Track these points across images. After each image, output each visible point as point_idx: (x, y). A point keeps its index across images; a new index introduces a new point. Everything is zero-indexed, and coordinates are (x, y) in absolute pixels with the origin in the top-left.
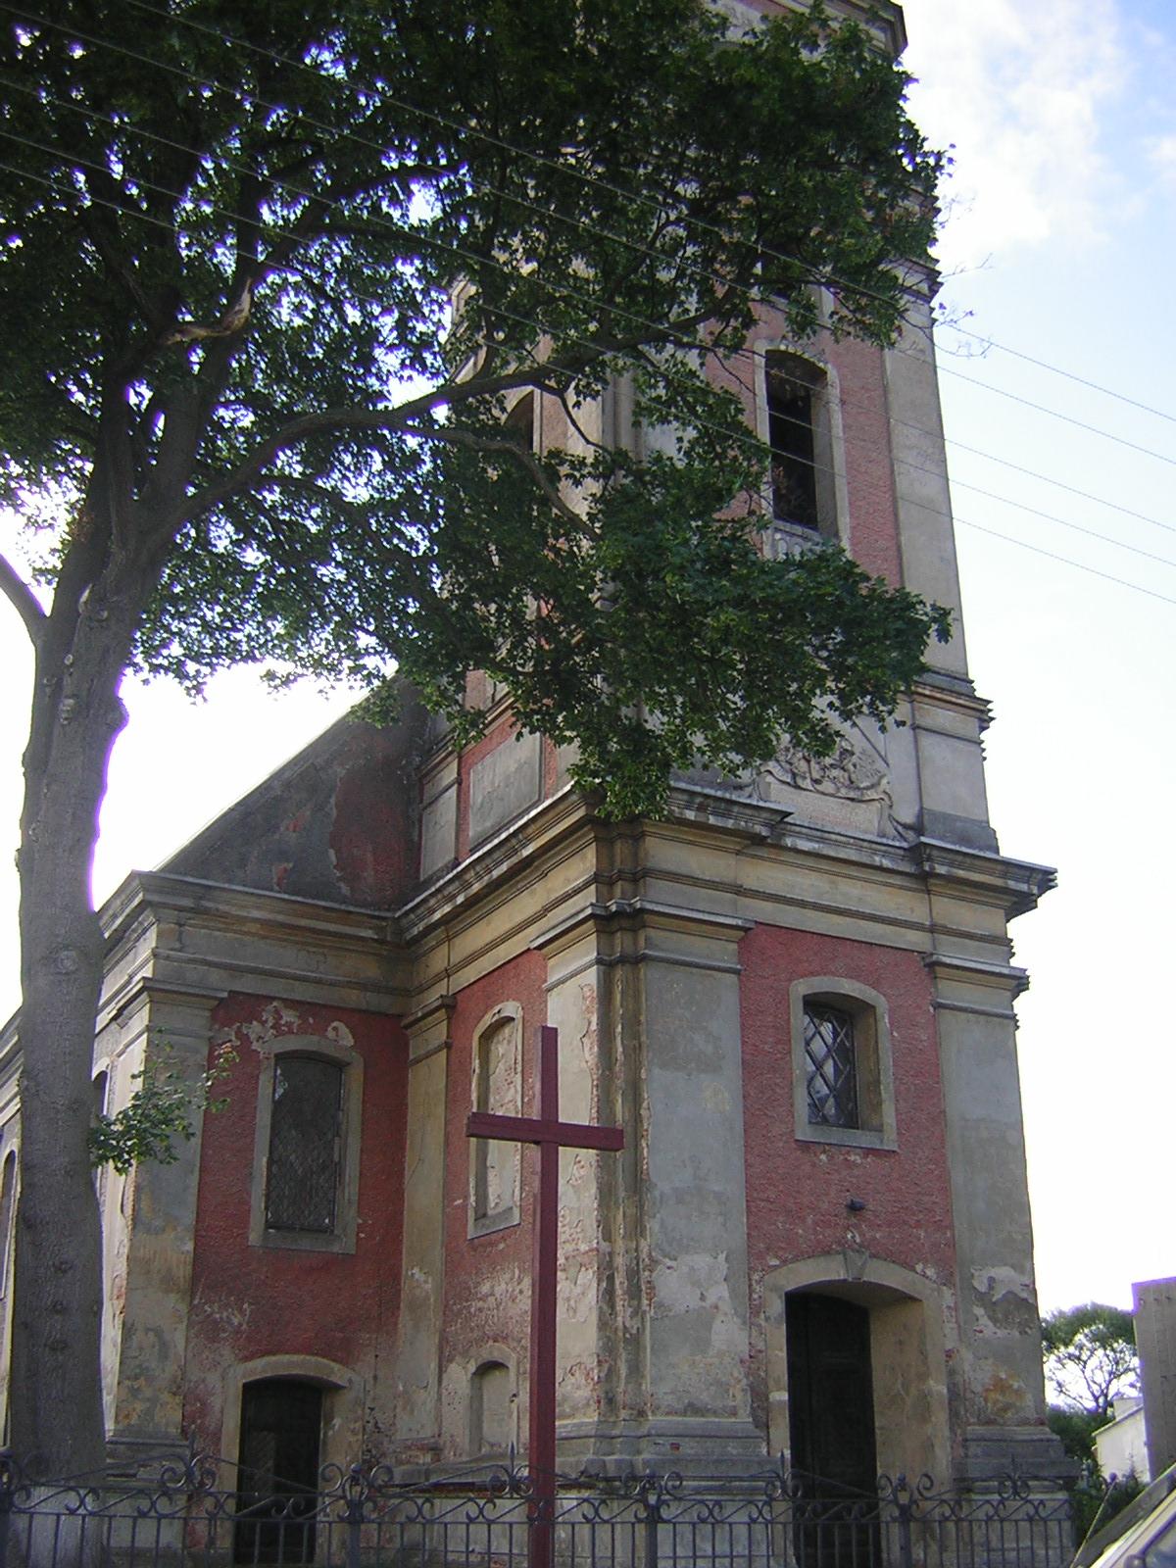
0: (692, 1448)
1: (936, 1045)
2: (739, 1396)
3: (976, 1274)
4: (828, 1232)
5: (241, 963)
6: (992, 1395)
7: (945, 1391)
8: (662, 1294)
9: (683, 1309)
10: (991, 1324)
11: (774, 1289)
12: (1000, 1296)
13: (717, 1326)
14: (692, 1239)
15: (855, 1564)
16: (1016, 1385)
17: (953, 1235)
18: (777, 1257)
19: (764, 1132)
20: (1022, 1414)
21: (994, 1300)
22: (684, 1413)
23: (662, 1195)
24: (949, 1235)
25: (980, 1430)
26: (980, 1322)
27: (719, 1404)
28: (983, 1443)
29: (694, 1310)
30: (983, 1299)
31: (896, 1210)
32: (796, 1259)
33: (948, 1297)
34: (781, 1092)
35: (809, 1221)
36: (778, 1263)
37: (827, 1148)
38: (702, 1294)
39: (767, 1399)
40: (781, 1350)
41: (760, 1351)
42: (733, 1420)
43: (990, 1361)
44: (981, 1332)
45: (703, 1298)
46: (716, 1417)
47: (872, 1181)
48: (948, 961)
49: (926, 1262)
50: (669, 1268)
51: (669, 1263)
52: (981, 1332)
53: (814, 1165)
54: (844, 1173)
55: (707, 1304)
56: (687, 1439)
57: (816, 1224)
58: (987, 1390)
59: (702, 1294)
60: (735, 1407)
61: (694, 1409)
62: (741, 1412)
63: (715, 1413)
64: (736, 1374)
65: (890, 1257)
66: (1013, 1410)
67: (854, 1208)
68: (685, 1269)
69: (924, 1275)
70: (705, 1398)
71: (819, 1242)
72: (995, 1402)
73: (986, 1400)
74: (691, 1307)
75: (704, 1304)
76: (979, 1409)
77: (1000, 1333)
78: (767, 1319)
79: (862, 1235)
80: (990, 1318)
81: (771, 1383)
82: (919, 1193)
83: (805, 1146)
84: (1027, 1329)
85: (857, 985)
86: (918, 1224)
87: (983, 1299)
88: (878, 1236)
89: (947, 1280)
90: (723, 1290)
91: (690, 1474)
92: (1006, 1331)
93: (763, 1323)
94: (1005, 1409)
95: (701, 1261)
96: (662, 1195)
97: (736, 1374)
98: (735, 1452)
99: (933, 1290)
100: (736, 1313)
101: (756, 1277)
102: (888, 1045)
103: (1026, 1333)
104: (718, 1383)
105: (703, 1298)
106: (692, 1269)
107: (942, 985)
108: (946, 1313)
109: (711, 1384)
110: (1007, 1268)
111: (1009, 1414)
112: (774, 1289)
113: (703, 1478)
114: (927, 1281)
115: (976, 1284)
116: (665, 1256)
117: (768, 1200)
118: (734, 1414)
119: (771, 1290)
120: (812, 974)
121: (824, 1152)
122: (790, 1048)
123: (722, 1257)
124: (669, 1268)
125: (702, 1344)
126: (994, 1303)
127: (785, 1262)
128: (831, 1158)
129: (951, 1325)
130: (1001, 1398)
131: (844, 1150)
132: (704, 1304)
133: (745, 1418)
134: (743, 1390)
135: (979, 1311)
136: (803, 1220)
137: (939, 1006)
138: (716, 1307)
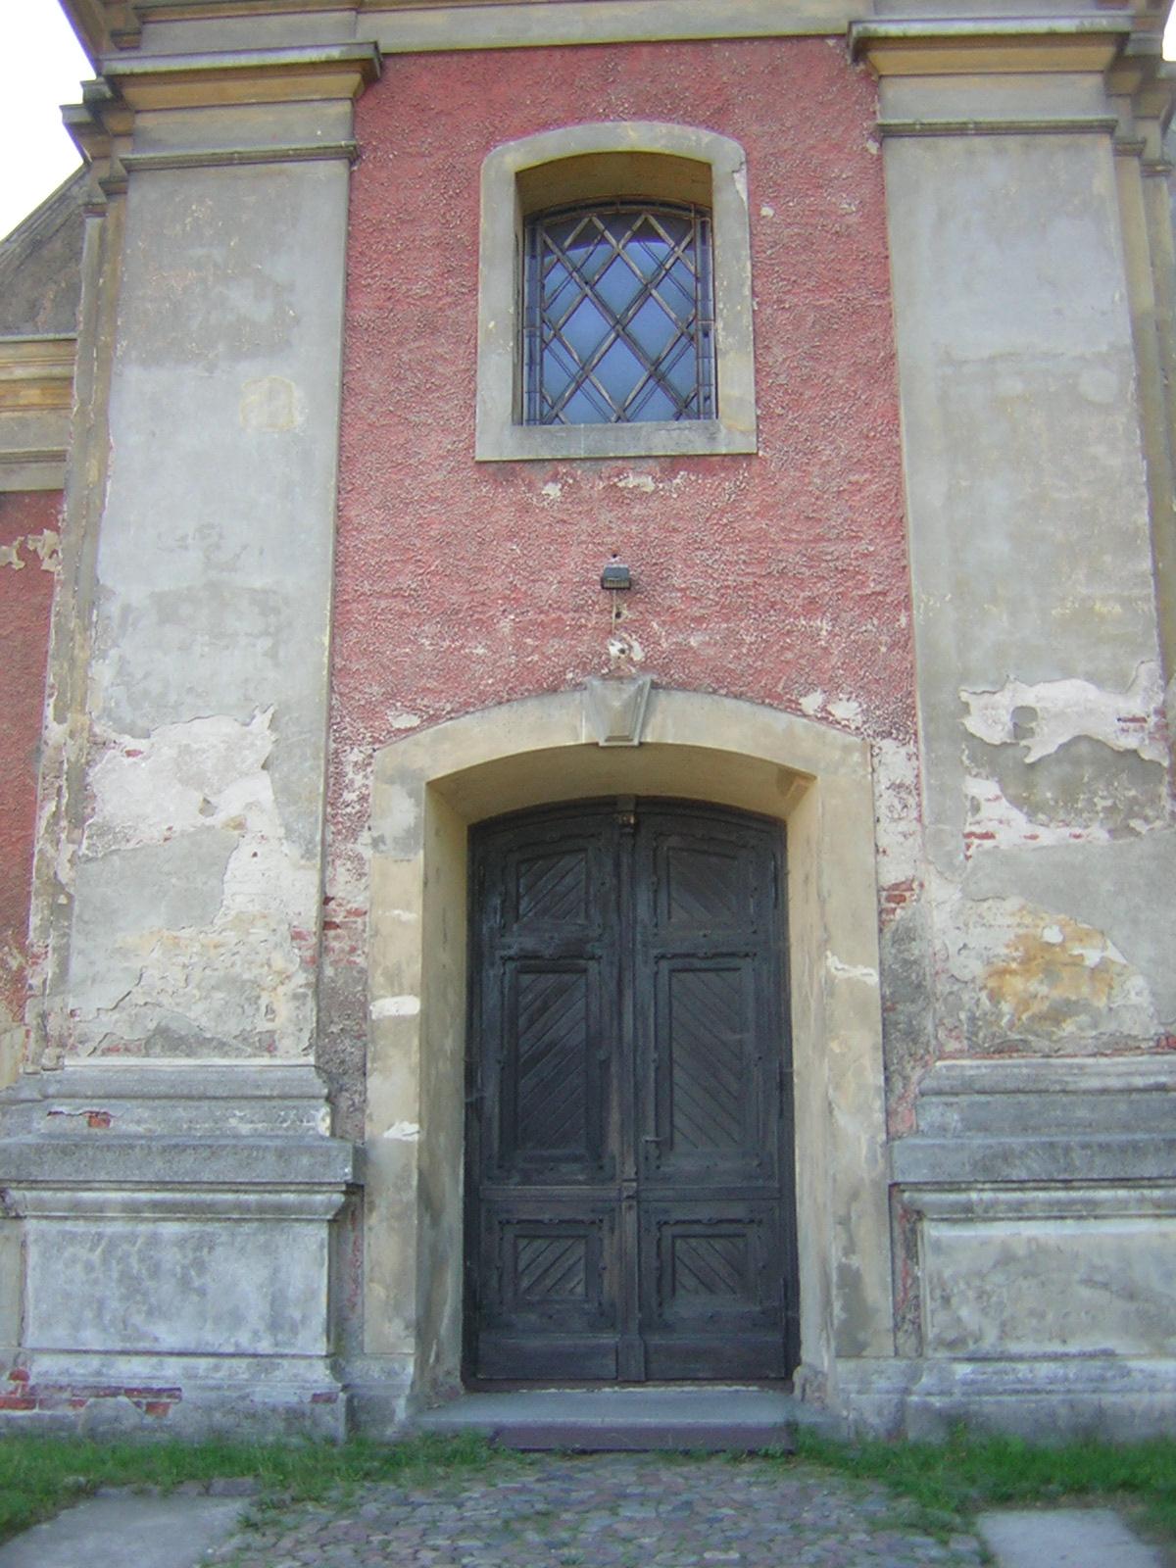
0: (139, 1122)
1: (876, 215)
2: (285, 1010)
3: (975, 703)
4: (554, 645)
5: (16, 450)
6: (1017, 984)
7: (874, 979)
8: (109, 809)
9: (158, 833)
10: (1018, 818)
11: (402, 776)
12: (1052, 749)
13: (240, 864)
14: (190, 690)
15: (7, 1141)
16: (1092, 957)
17: (910, 625)
18: (413, 710)
19: (399, 458)
20: (1109, 1027)
21: (1029, 760)
22: (146, 1047)
23: (126, 610)
24: (903, 621)
25: (971, 1066)
26: (982, 815)
27: (232, 1027)
28: (963, 1100)
29: (183, 834)
30: (989, 757)
31: (748, 580)
32: (463, 709)
33: (896, 760)
34: (449, 370)
35: (505, 625)
36: (415, 721)
37: (563, 469)
38: (206, 801)
39: (366, 1016)
40: (408, 907)
41: (359, 913)
42: (266, 1061)
43: (1012, 903)
44: (988, 836)
45: (207, 808)
46: (226, 1055)
47: (680, 525)
48: (894, 30)
49: (832, 687)
50: (129, 754)
51: (128, 742)
52: (988, 836)
53: (525, 509)
54: (605, 517)
55: (218, 819)
56: (128, 1104)
57: (521, 630)
58: (1003, 973)
59: (206, 801)
60: (271, 1033)
61: (169, 1039)
62: (285, 1044)
63: (221, 1047)
64: (279, 962)
65: (724, 683)
66: (1084, 1018)
67: (619, 585)
68: (168, 752)
69: (825, 717)
70: (198, 1015)
71: (530, 668)
72: (1025, 1002)
73: (995, 997)
74: (177, 828)
75: (209, 821)
76: (973, 1019)
77: (1050, 836)
78: (377, 842)
79: (648, 640)
80: (1017, 802)
81: (378, 979)
82: (819, 539)
83: (505, 471)
84: (1135, 823)
85: (661, 128)
86: (812, 607)
87: (989, 757)
88: (693, 642)
89: (897, 725)
90: (262, 788)
91: (103, 1176)
92: (1066, 831)
93: (368, 853)
94: (1059, 1013)
95: (211, 733)
96: (126, 610)
97: (279, 962)
98: (245, 1129)
99: (847, 749)
100: (289, 831)
101: (355, 756)
102: (742, 235)
103: (1132, 832)
104: (232, 982)
105: (207, 808)
106: (185, 750)
107: (892, 91)
108: (888, 798)
109: (215, 988)
110: (1078, 683)
111: (1069, 1027)
112: (402, 776)
113: (139, 1185)
114: (833, 733)
115: (973, 724)
116: (122, 731)
117: (397, 594)
118: (270, 1048)
119: (391, 781)
120: (545, 126)
121: (555, 478)
122: (476, 284)
123: (262, 721)
124: (129, 754)
125: (198, 905)
126: (1032, 766)
127: (433, 719)
128: (571, 490)
129: (903, 826)
130: (1044, 990)
131: (606, 468)
132: (209, 821)
133: (295, 1057)
134: (295, 997)
135: (982, 788)
136: (486, 626)
137: (886, 133)
138: (240, 825)
